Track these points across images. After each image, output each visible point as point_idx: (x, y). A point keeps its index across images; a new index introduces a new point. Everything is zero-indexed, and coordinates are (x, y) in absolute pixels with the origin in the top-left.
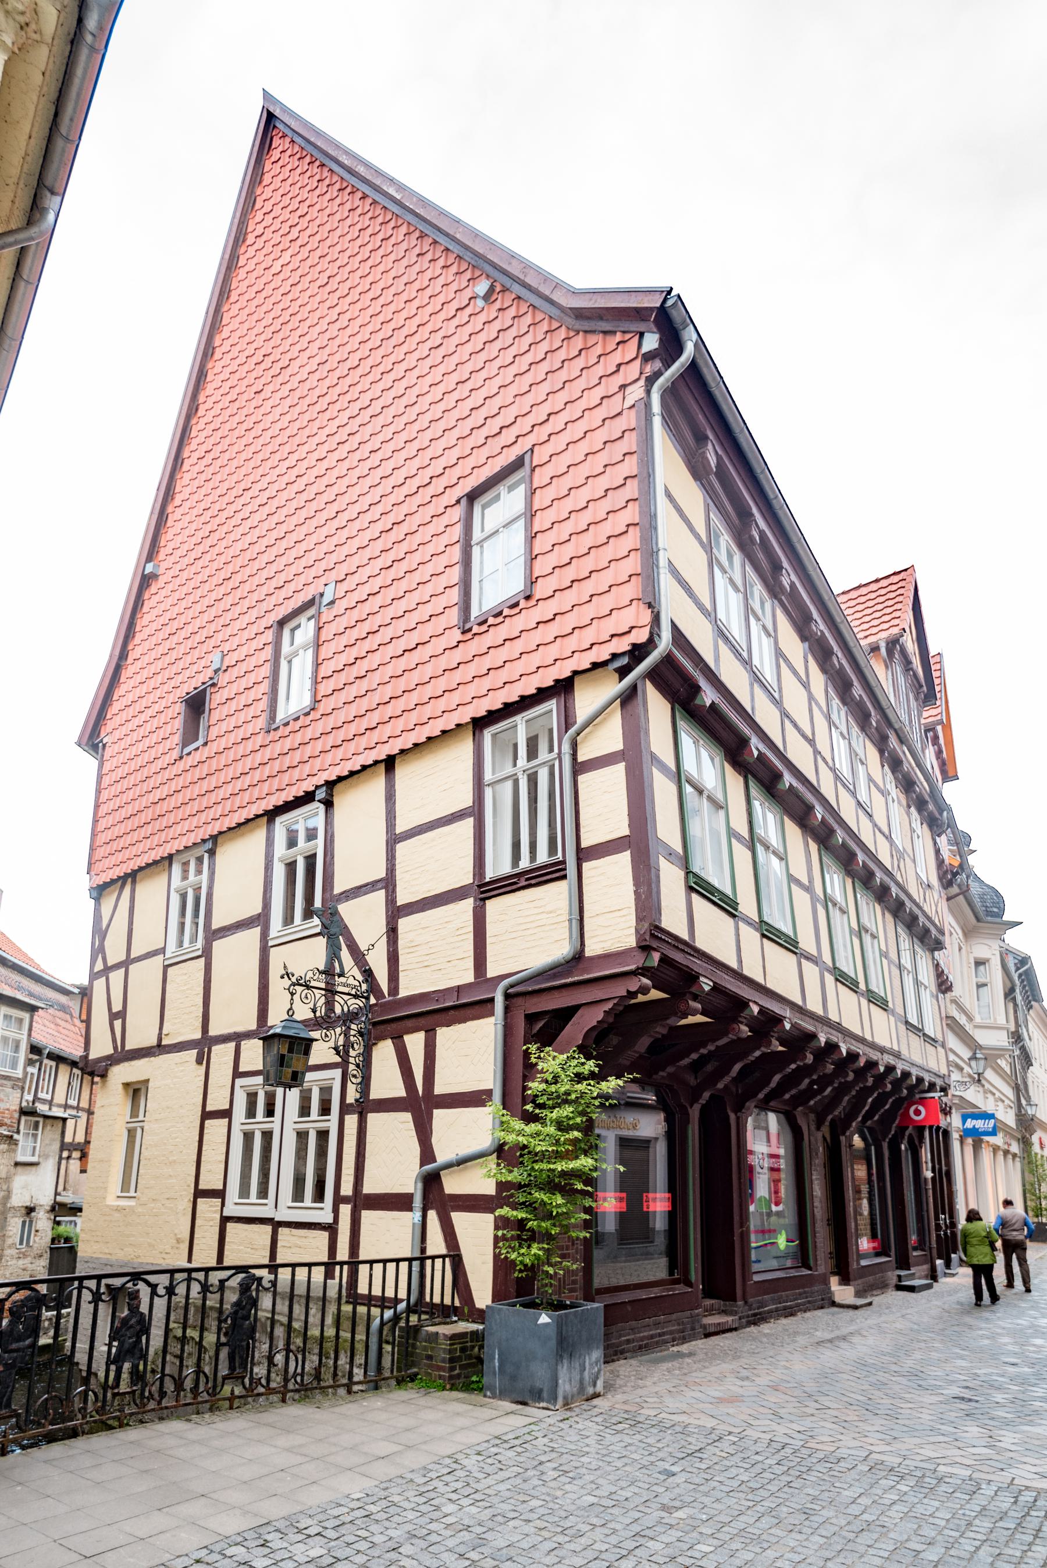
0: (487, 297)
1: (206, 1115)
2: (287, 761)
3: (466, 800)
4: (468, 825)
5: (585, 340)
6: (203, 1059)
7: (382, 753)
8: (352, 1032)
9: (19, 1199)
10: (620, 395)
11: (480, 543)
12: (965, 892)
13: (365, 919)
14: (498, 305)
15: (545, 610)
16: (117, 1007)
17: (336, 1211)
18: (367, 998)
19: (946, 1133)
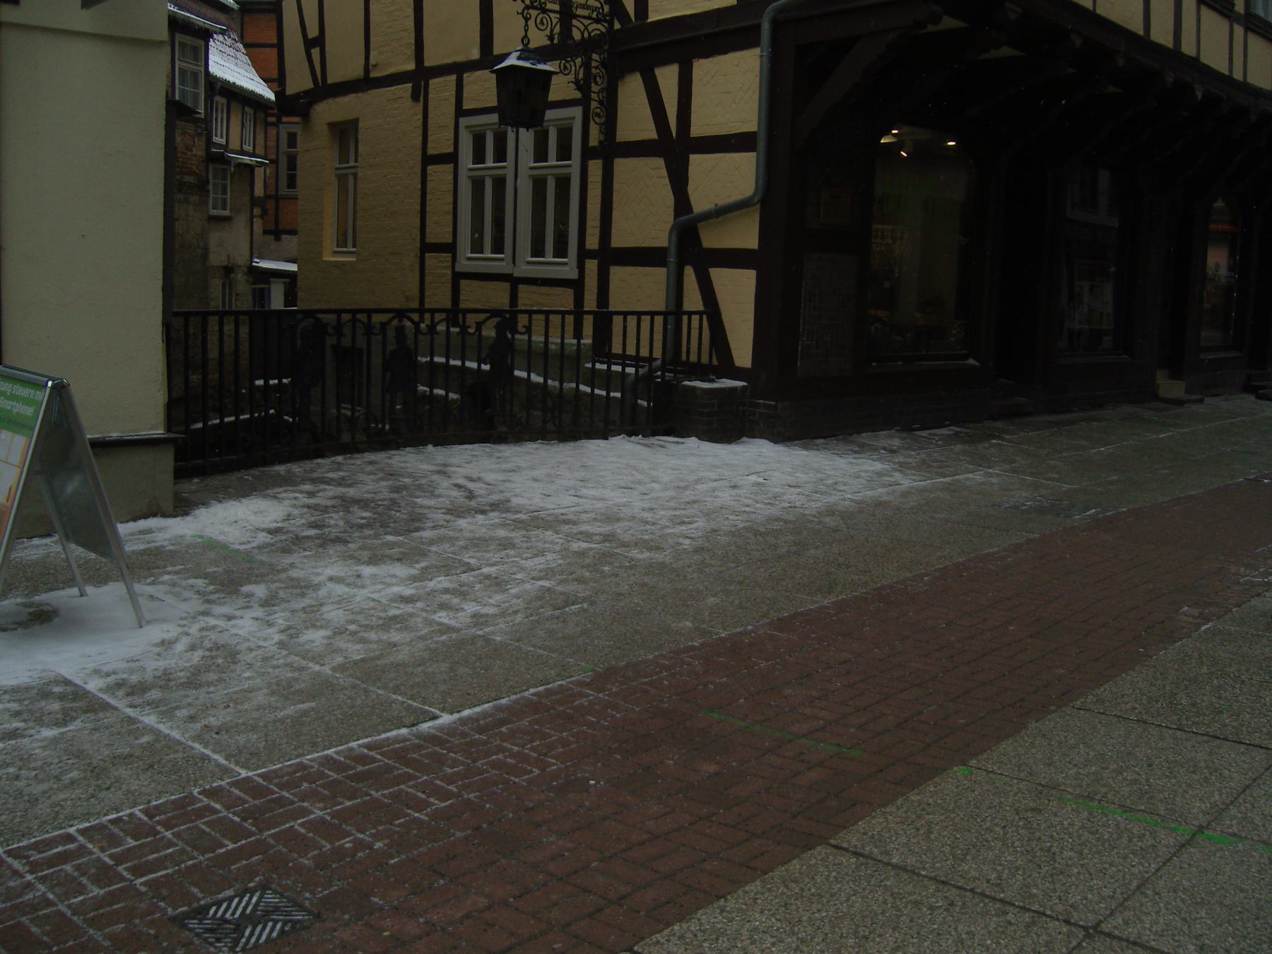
1: (428, 160)
6: (421, 94)
8: (594, 64)
9: (217, 259)
16: (313, 32)
18: (611, 23)
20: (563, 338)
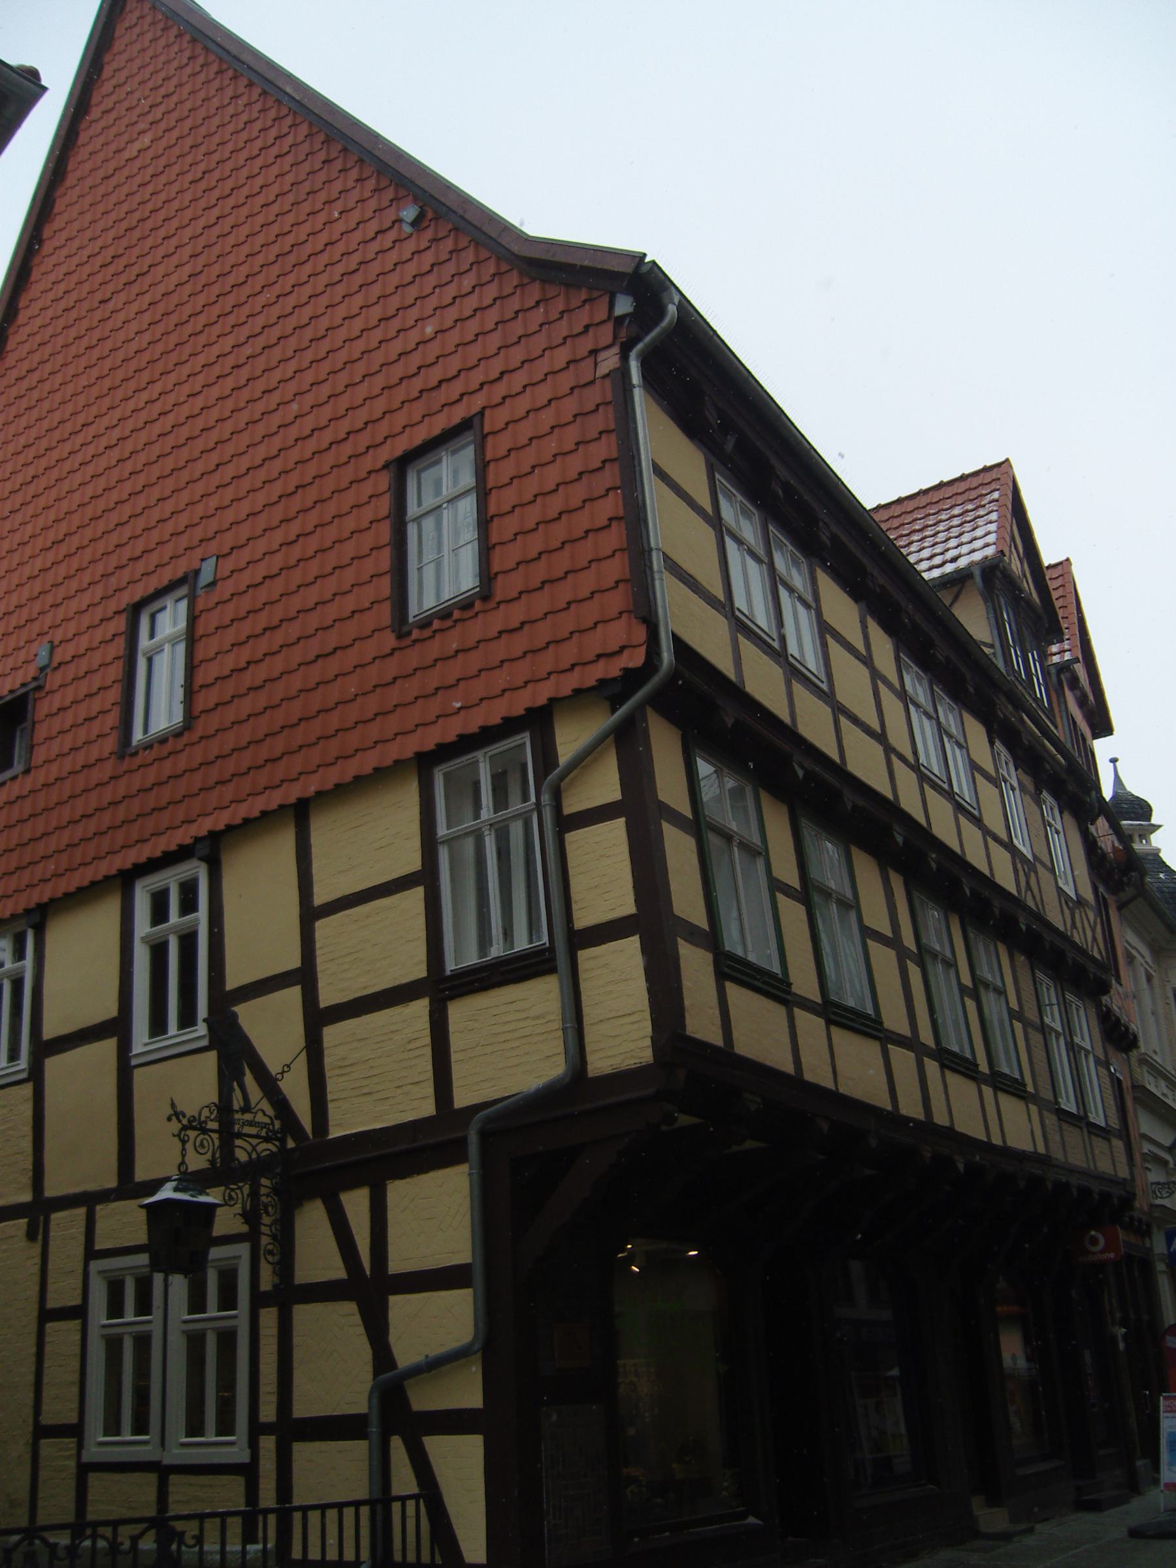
0: (415, 223)
1: (46, 1315)
2: (151, 800)
3: (412, 862)
4: (415, 897)
5: (543, 290)
6: (38, 1232)
7: (293, 793)
8: (263, 1191)
10: (590, 361)
11: (418, 519)
12: (1142, 891)
13: (274, 1028)
14: (429, 234)
15: (516, 613)
17: (253, 1445)
18: (283, 1141)
19: (1146, 1265)
20: (223, 1544)
